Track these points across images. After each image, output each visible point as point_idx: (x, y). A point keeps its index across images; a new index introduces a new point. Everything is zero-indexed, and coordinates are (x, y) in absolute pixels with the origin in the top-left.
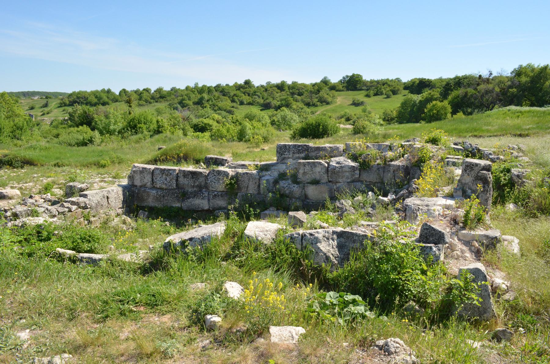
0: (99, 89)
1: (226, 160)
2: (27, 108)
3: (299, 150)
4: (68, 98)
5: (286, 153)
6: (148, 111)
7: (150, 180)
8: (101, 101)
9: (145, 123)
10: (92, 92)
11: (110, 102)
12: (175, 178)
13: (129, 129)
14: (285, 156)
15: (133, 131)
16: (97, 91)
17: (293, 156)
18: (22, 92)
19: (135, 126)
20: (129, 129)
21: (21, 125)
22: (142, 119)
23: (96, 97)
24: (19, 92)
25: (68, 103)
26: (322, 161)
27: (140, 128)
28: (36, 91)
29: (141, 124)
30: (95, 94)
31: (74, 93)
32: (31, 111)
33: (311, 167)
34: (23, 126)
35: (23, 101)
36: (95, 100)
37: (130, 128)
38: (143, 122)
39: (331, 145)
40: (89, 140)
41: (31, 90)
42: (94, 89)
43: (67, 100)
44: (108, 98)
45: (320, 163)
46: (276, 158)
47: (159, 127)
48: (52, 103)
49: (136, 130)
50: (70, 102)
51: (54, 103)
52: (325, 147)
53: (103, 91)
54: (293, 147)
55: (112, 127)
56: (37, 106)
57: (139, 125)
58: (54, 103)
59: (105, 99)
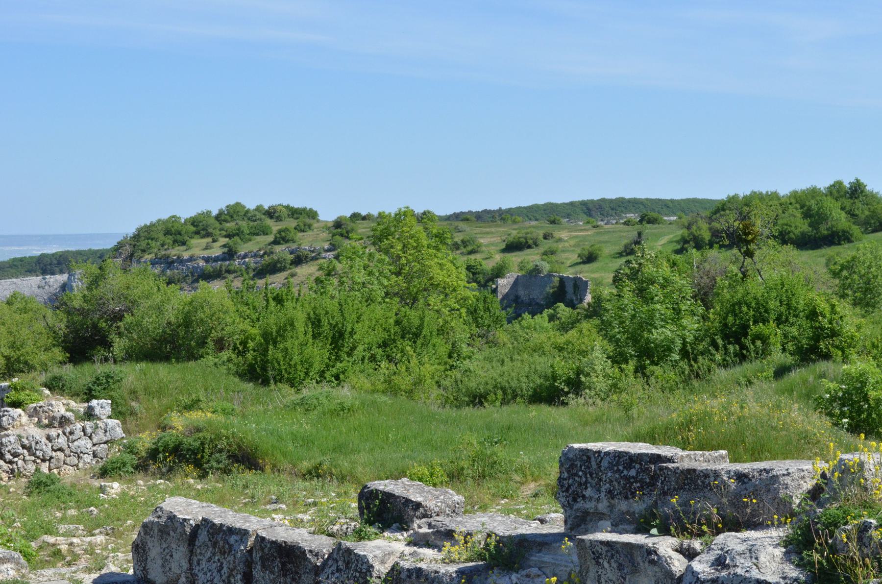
0: (823, 183)
1: (418, 505)
2: (574, 258)
3: (627, 478)
4: (710, 219)
5: (588, 492)
6: (777, 268)
7: (185, 566)
8: (824, 230)
9: (779, 321)
10: (794, 194)
11: (856, 230)
12: (241, 567)
13: (720, 342)
14: (590, 506)
15: (731, 348)
16: (813, 192)
17: (611, 507)
18: (584, 203)
19: (745, 328)
20: (720, 342)
21: (416, 322)
22: (773, 304)
23: (807, 214)
24: (572, 204)
25: (707, 236)
26: (665, 546)
27: (758, 337)
28: (628, 196)
29: (765, 321)
30: (807, 204)
31: (733, 199)
32: (586, 267)
33: (620, 567)
34: (421, 327)
35: (564, 235)
36: (801, 226)
37: (725, 337)
38: (773, 316)
39: (744, 467)
40: (569, 382)
41: (612, 194)
42: (801, 184)
43: (705, 226)
44: (852, 214)
45: (650, 552)
46: (560, 516)
47: (818, 335)
48: (658, 237)
49: (743, 347)
50: (715, 234)
51: (664, 240)
52: (716, 474)
53: (836, 190)
54: (611, 467)
55: (658, 335)
56: (608, 250)
57: (754, 329)
58: (664, 240)
59: (840, 219)
